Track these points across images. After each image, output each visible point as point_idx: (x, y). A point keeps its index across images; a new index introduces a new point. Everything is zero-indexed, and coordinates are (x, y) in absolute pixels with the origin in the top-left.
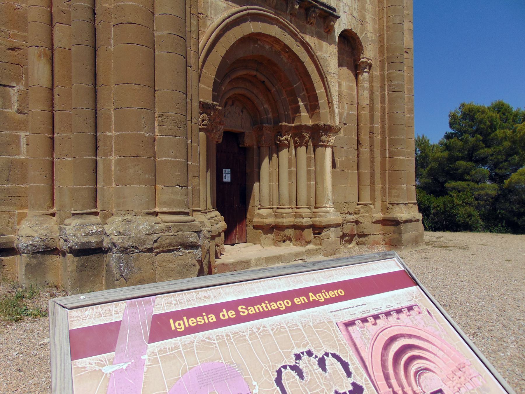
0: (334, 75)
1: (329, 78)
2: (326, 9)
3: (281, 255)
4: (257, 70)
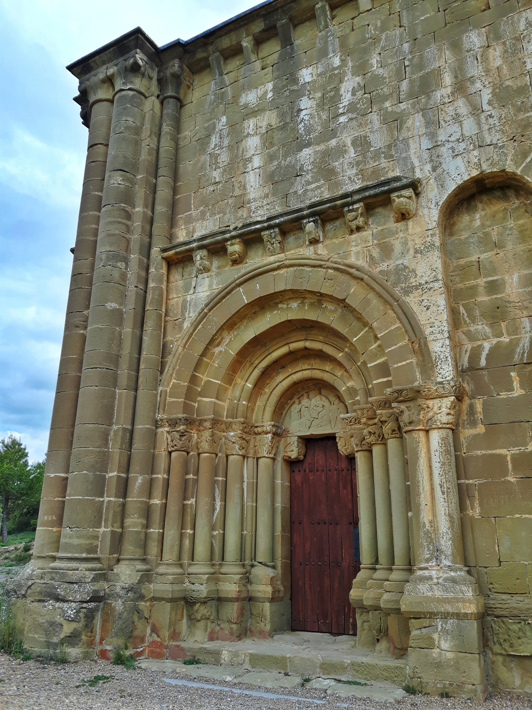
0: (431, 285)
1: (412, 301)
2: (372, 192)
3: (284, 659)
4: (306, 340)
